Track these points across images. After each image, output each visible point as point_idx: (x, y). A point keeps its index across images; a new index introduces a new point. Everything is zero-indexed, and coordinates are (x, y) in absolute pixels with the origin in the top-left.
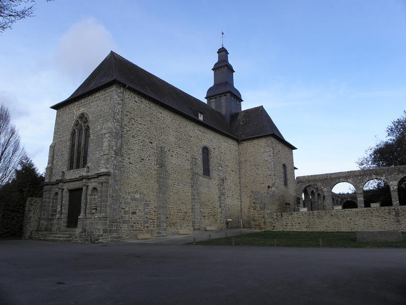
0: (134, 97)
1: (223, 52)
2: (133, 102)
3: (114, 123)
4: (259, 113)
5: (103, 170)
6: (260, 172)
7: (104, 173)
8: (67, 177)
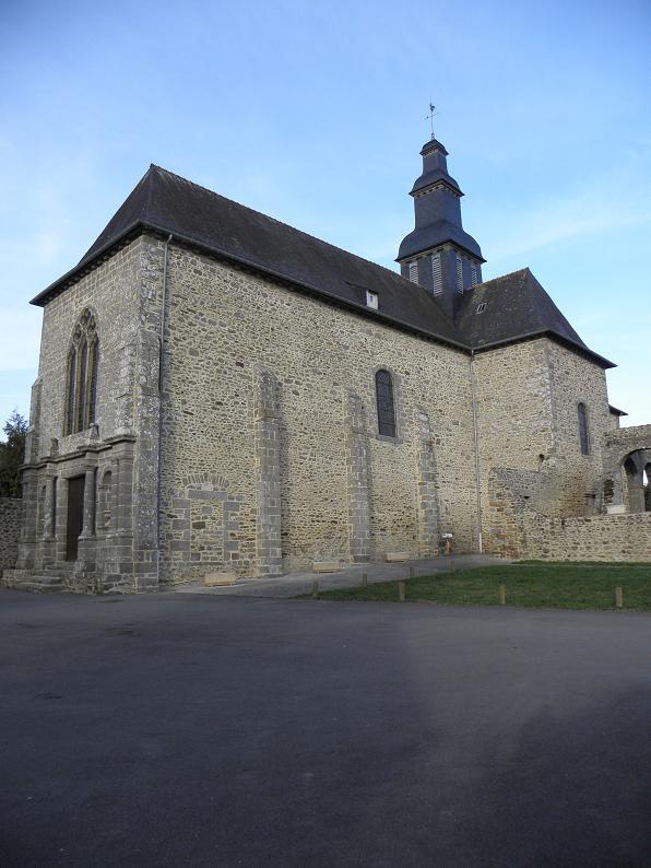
0: (193, 263)
1: (434, 153)
2: (190, 271)
3: (143, 323)
4: (523, 285)
5: (120, 431)
6: (520, 422)
7: (119, 436)
8: (63, 451)
